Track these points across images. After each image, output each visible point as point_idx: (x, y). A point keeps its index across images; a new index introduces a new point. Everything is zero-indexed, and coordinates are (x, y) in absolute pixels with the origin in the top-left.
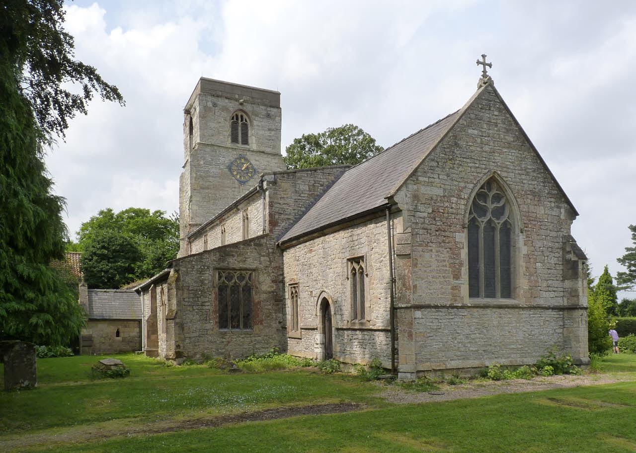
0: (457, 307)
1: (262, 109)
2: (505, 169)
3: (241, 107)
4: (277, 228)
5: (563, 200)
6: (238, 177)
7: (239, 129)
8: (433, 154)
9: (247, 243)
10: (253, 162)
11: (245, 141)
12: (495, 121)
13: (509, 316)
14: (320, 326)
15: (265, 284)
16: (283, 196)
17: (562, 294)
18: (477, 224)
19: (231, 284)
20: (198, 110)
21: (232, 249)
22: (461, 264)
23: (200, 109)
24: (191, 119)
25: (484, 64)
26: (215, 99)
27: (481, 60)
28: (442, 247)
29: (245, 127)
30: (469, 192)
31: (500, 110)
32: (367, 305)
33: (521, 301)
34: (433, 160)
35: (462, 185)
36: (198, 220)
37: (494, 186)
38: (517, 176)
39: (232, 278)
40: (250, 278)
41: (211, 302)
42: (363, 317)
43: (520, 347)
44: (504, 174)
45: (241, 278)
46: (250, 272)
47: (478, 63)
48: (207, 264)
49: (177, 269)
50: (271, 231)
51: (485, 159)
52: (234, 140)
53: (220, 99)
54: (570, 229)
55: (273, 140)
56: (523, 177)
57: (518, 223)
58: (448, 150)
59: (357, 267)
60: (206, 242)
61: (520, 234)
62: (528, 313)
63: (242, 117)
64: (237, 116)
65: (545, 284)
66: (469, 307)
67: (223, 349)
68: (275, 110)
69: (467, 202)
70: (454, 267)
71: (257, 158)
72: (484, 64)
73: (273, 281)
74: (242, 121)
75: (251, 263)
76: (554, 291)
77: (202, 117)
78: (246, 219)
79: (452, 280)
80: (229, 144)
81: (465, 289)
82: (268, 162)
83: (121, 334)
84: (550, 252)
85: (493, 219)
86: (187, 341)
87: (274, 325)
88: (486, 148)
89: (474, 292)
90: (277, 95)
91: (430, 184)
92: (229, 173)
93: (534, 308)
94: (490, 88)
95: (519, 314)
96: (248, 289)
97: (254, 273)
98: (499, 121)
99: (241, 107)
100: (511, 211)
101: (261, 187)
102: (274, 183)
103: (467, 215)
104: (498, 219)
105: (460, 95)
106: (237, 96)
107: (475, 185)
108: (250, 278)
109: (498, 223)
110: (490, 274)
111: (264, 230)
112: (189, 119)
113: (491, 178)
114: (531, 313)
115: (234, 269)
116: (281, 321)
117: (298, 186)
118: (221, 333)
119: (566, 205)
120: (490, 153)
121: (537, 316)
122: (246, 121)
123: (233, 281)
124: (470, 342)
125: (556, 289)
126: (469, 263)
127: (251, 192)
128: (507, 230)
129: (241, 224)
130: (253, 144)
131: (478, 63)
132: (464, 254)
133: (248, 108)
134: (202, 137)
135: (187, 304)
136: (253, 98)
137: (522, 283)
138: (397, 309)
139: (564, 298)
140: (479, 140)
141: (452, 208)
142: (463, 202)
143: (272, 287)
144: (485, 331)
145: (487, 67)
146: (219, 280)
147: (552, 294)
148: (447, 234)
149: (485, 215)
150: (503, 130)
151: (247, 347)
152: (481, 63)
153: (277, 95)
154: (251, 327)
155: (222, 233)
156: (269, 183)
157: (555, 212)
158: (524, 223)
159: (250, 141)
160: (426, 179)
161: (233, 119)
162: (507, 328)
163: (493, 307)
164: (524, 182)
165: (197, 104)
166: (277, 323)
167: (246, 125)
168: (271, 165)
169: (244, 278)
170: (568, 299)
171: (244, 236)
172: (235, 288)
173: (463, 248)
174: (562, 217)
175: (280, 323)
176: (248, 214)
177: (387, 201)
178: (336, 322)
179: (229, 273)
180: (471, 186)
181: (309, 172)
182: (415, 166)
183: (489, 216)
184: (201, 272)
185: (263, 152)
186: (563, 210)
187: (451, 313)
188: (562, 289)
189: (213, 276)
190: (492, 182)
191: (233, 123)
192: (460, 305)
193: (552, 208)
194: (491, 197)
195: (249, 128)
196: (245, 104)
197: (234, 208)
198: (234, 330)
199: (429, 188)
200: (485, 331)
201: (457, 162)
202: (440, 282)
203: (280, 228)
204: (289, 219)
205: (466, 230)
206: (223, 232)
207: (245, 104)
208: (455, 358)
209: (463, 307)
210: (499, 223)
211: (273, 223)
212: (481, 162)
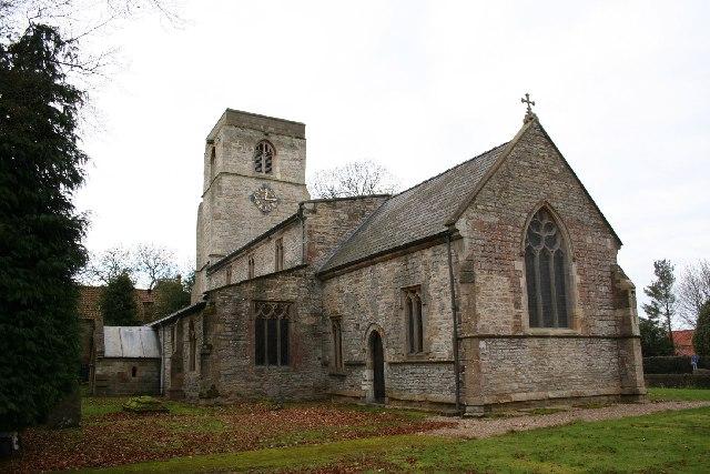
3: (265, 137)
6: (261, 206)
7: (264, 153)
14: (369, 361)
15: (304, 318)
25: (529, 102)
30: (524, 219)
31: (546, 144)
32: (426, 336)
33: (579, 332)
39: (269, 310)
41: (248, 339)
42: (421, 349)
44: (555, 205)
45: (279, 310)
59: (412, 297)
60: (229, 275)
64: (261, 146)
68: (297, 142)
78: (280, 248)
86: (223, 378)
90: (302, 126)
93: (590, 337)
99: (265, 137)
104: (551, 247)
105: (507, 129)
110: (548, 303)
115: (272, 301)
131: (523, 101)
132: (523, 281)
133: (273, 138)
138: (461, 339)
153: (302, 126)
172: (273, 321)
177: (446, 229)
178: (389, 355)
183: (543, 245)
190: (545, 211)
209: (525, 337)
210: (552, 252)
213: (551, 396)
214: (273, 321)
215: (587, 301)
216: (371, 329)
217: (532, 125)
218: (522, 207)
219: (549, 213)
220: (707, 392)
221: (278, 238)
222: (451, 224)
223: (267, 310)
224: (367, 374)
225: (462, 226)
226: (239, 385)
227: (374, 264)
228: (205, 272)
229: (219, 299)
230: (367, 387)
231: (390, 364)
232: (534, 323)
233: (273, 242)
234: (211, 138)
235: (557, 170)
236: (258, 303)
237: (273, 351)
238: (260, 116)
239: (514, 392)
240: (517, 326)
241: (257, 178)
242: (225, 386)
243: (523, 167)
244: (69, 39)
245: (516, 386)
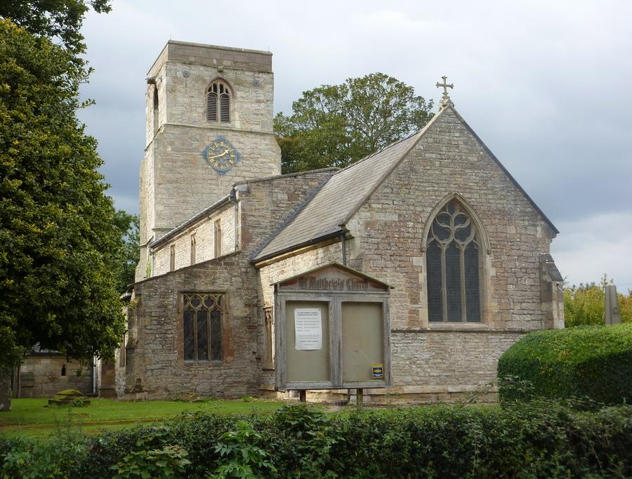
0: (414, 331)
1: (248, 76)
2: (468, 190)
3: (220, 75)
4: (250, 244)
5: (539, 217)
6: (216, 165)
7: (218, 99)
8: (386, 181)
9: (217, 261)
10: (236, 145)
11: (226, 118)
12: (456, 143)
13: (474, 341)
15: (237, 308)
16: (257, 207)
17: (540, 317)
18: (438, 246)
19: (198, 308)
20: (164, 81)
21: (199, 270)
22: (419, 288)
23: (168, 82)
24: (156, 91)
25: (445, 86)
26: (186, 68)
27: (442, 82)
28: (398, 272)
29: (226, 99)
30: (428, 215)
33: (491, 326)
34: (387, 187)
35: (419, 209)
36: (164, 224)
37: (457, 207)
38: (482, 196)
40: (219, 302)
41: (174, 329)
43: (489, 373)
44: (467, 195)
45: (209, 301)
46: (219, 295)
47: (438, 85)
48: (171, 287)
49: (138, 293)
50: (244, 247)
52: (211, 116)
53: (192, 66)
54: (548, 248)
55: (262, 115)
56: (490, 197)
57: (486, 242)
58: (403, 176)
61: (487, 255)
62: (497, 337)
63: (221, 87)
64: (215, 86)
65: (518, 307)
66: (428, 331)
67: (189, 383)
69: (425, 226)
70: (411, 291)
71: (242, 140)
72: (445, 86)
73: (246, 305)
74: (221, 92)
75: (222, 285)
76: (530, 314)
77: (171, 90)
78: (218, 232)
79: (409, 304)
80: (205, 123)
82: (256, 144)
83: (68, 372)
84: (524, 273)
85: (457, 241)
86: (149, 373)
87: (248, 356)
88: (446, 171)
89: (435, 315)
90: (267, 57)
91: (383, 210)
92: (204, 160)
93: (505, 332)
94: (449, 110)
95: (487, 338)
96: (217, 314)
97: (223, 297)
98: (461, 143)
99: (220, 75)
100: (477, 232)
101: (233, 197)
102: (248, 192)
103: (425, 239)
104: (463, 240)
106: (215, 62)
107: (434, 209)
108: (219, 302)
109: (463, 245)
111: (237, 246)
112: (153, 90)
113: (453, 200)
114: (503, 337)
115: (201, 292)
116: (255, 351)
117: (275, 195)
118: (186, 365)
119: (543, 223)
120: (451, 175)
121: (510, 340)
122: (227, 92)
123: (200, 306)
124: (430, 367)
125: (532, 312)
126: (428, 287)
127: (222, 202)
128: (474, 253)
129: (213, 237)
130: (237, 122)
131: (438, 85)
132: (423, 277)
133: (230, 75)
134: (170, 116)
135: (149, 332)
136: (236, 62)
137: (491, 304)
139: (543, 322)
140: (437, 164)
141: (408, 233)
142: (420, 226)
143: (246, 312)
144: (447, 356)
145: (448, 89)
146: (185, 304)
147: (528, 318)
148: (403, 258)
149: (448, 237)
150: (465, 151)
151: (215, 380)
152: (442, 85)
153: (267, 57)
154: (220, 359)
155: (192, 244)
156: (241, 193)
157: (531, 231)
158: (491, 244)
159: (232, 118)
160: (380, 206)
161: (210, 90)
162: (474, 353)
163: (456, 331)
164: (491, 201)
165: (163, 73)
166: (251, 354)
167: (227, 97)
168: (260, 147)
169: (212, 301)
170: (545, 323)
171: (191, 263)
172: (203, 314)
173: (421, 271)
174: (539, 235)
175: (254, 353)
176: (221, 226)
179: (209, 298)
180: (429, 209)
181: (289, 179)
182: (366, 192)
183: (452, 238)
184: (164, 295)
185: (251, 132)
186: (539, 229)
187: (408, 337)
188: (540, 312)
189: (179, 300)
190: (454, 203)
191: (211, 95)
192: (418, 329)
193: (525, 227)
194: (453, 218)
195: (231, 101)
196: (225, 71)
197: (206, 215)
198: (201, 361)
199: (382, 214)
200: (447, 356)
201: (412, 187)
202: (395, 306)
203: (255, 244)
204: (264, 233)
205: (424, 254)
206: (193, 244)
207: (225, 71)
208: (414, 383)
209: (423, 331)
211: (246, 237)
212: (440, 185)
213: (450, 389)
218: (427, 206)
219: (460, 203)
221: (217, 218)
222: (343, 226)
223: (196, 302)
226: (167, 380)
227: (294, 255)
232: (432, 318)
233: (213, 221)
234: (150, 76)
235: (473, 159)
236: (191, 295)
237: (202, 345)
238: (212, 48)
239: (408, 384)
242: (150, 381)
243: (431, 162)
245: (409, 379)
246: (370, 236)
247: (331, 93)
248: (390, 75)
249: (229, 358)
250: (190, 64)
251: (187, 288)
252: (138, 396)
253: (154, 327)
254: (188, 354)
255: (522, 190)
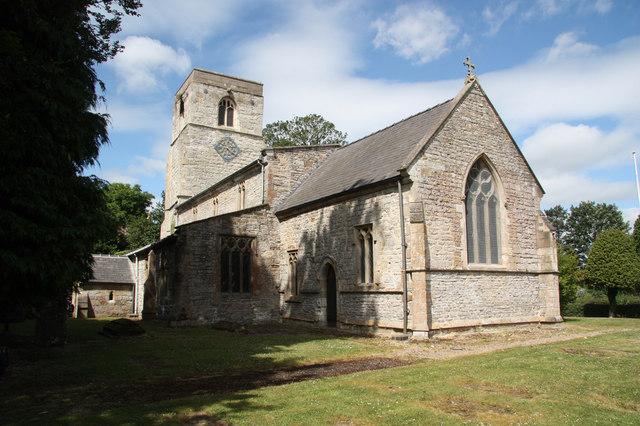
1: (247, 97)
11: (230, 123)
14: (323, 290)
19: (233, 249)
26: (206, 87)
29: (231, 110)
37: (482, 164)
41: (213, 266)
44: (489, 156)
45: (242, 244)
51: (410, 378)
52: (221, 122)
59: (364, 233)
80: (215, 125)
81: (464, 254)
130: (236, 126)
132: (463, 222)
148: (449, 205)
172: (236, 254)
177: (398, 174)
180: (466, 164)
184: (206, 237)
214: (236, 254)
215: (514, 242)
216: (325, 262)
217: (473, 85)
220: (638, 320)
223: (231, 244)
224: (323, 301)
225: (413, 173)
228: (174, 210)
229: (189, 234)
230: (321, 315)
231: (342, 293)
232: (470, 259)
235: (493, 126)
240: (458, 262)
241: (221, 130)
244: (246, 188)
246: (424, 182)
247: (284, 126)
248: (326, 119)
249: (258, 292)
250: (209, 85)
251: (224, 232)
252: (183, 323)
253: (197, 264)
254: (225, 288)
255: (523, 157)
